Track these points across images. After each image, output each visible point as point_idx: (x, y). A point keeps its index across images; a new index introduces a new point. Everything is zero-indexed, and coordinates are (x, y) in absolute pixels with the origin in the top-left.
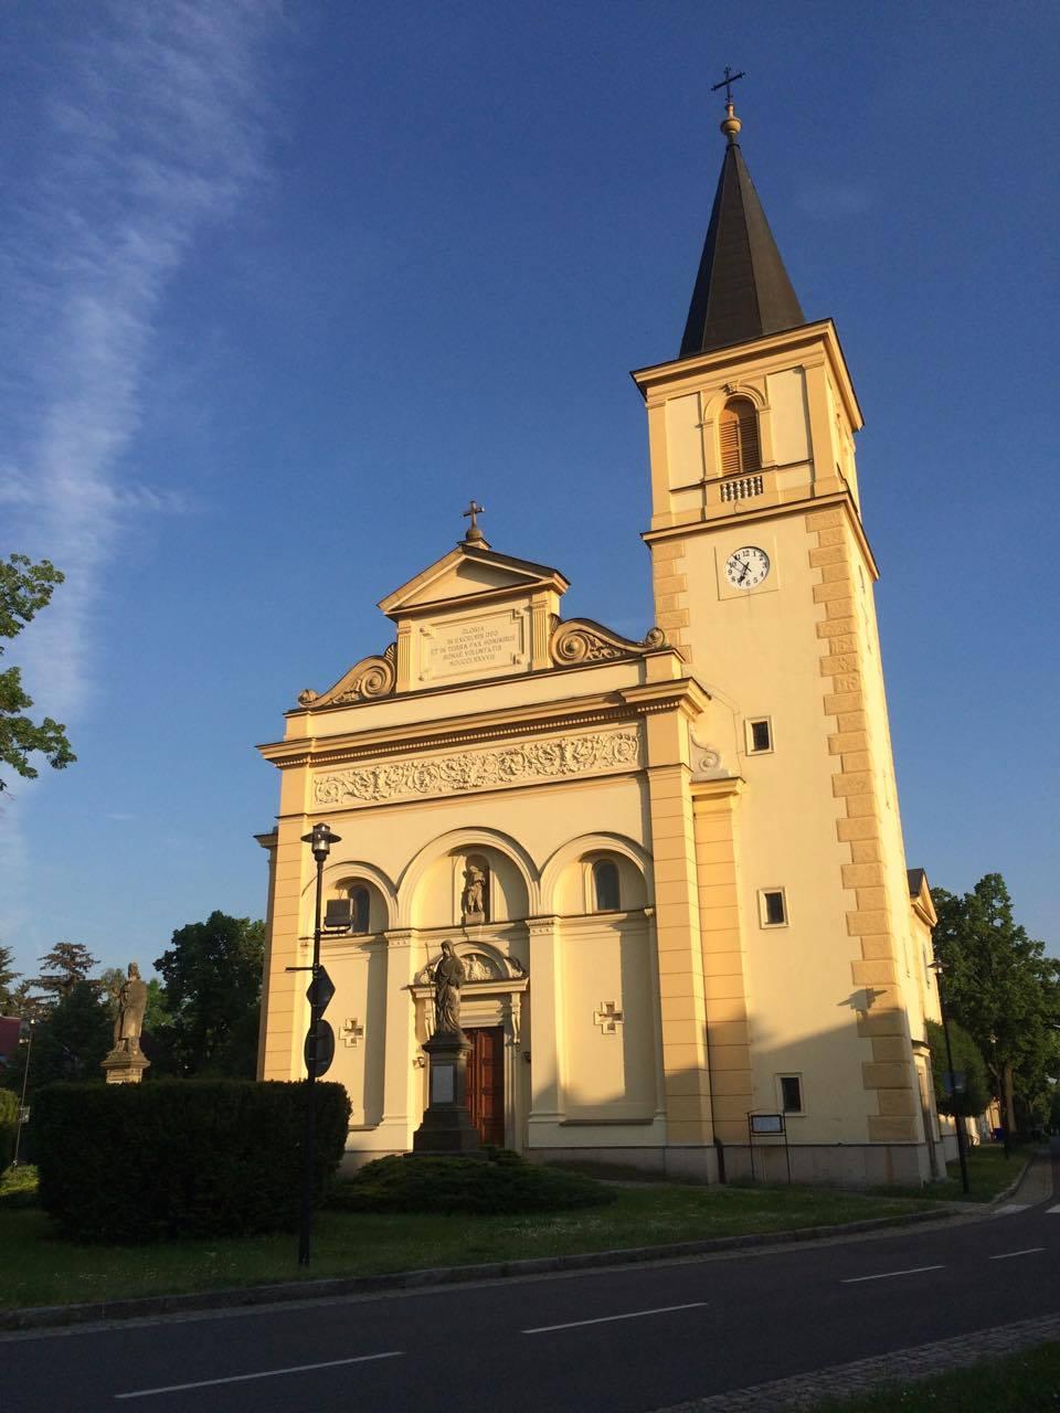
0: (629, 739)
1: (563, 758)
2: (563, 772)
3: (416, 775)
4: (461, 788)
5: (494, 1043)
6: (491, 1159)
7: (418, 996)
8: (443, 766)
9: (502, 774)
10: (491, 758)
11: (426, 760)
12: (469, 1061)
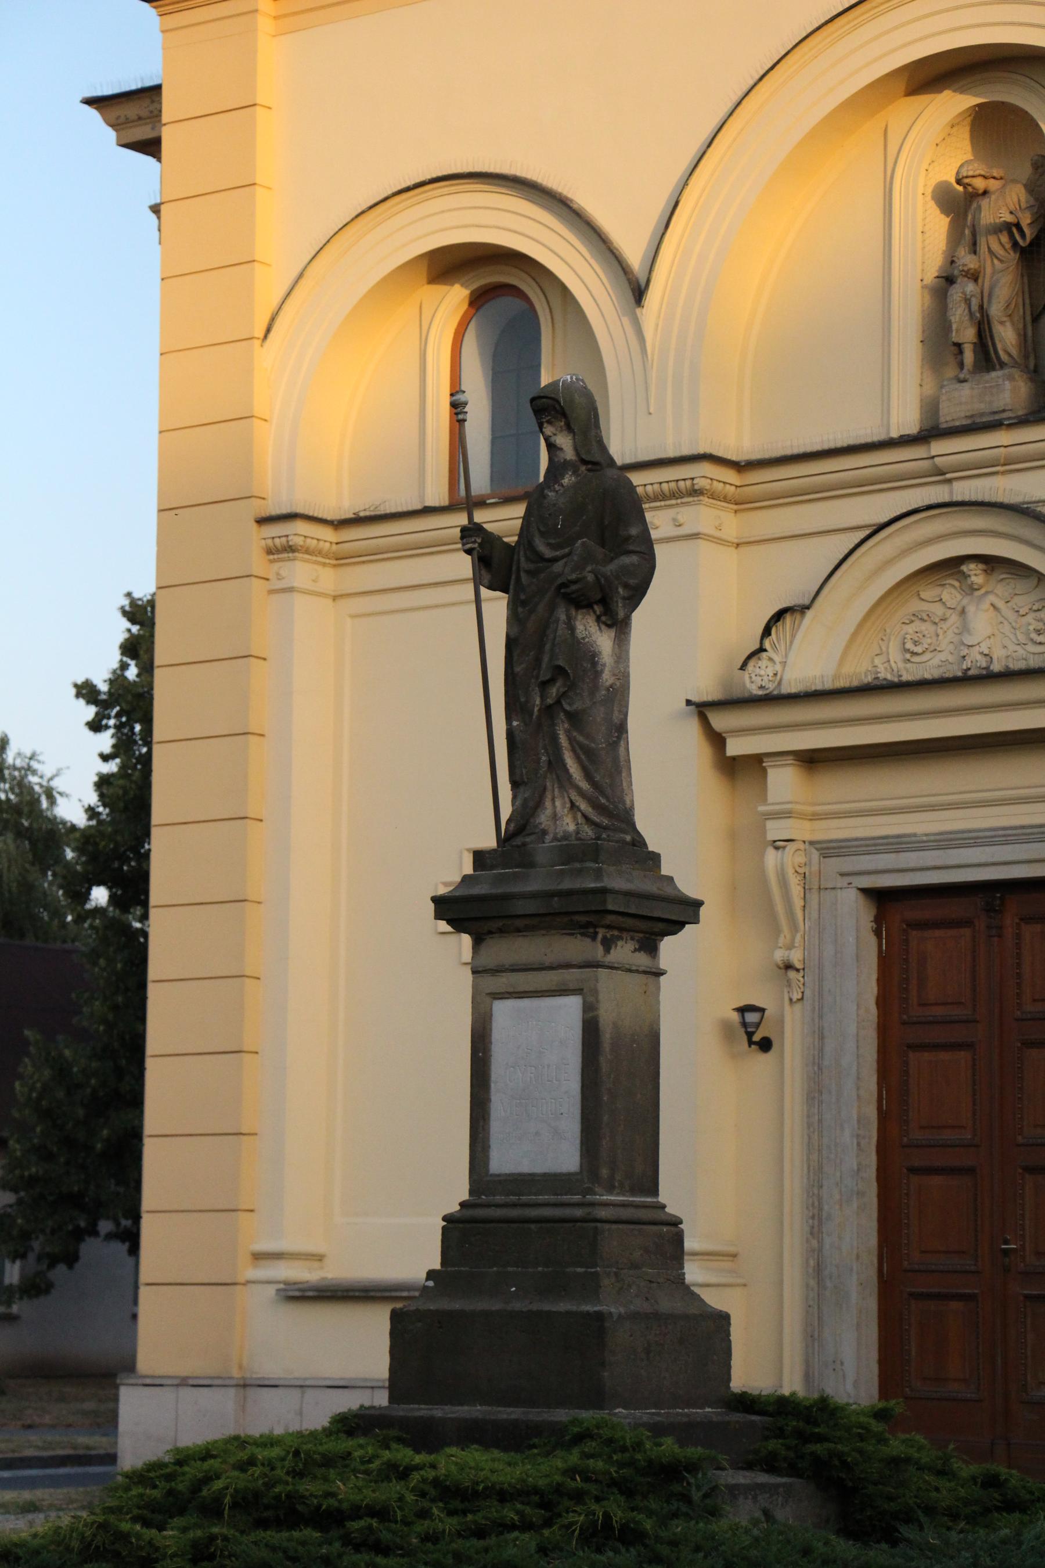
7: (735, 747)
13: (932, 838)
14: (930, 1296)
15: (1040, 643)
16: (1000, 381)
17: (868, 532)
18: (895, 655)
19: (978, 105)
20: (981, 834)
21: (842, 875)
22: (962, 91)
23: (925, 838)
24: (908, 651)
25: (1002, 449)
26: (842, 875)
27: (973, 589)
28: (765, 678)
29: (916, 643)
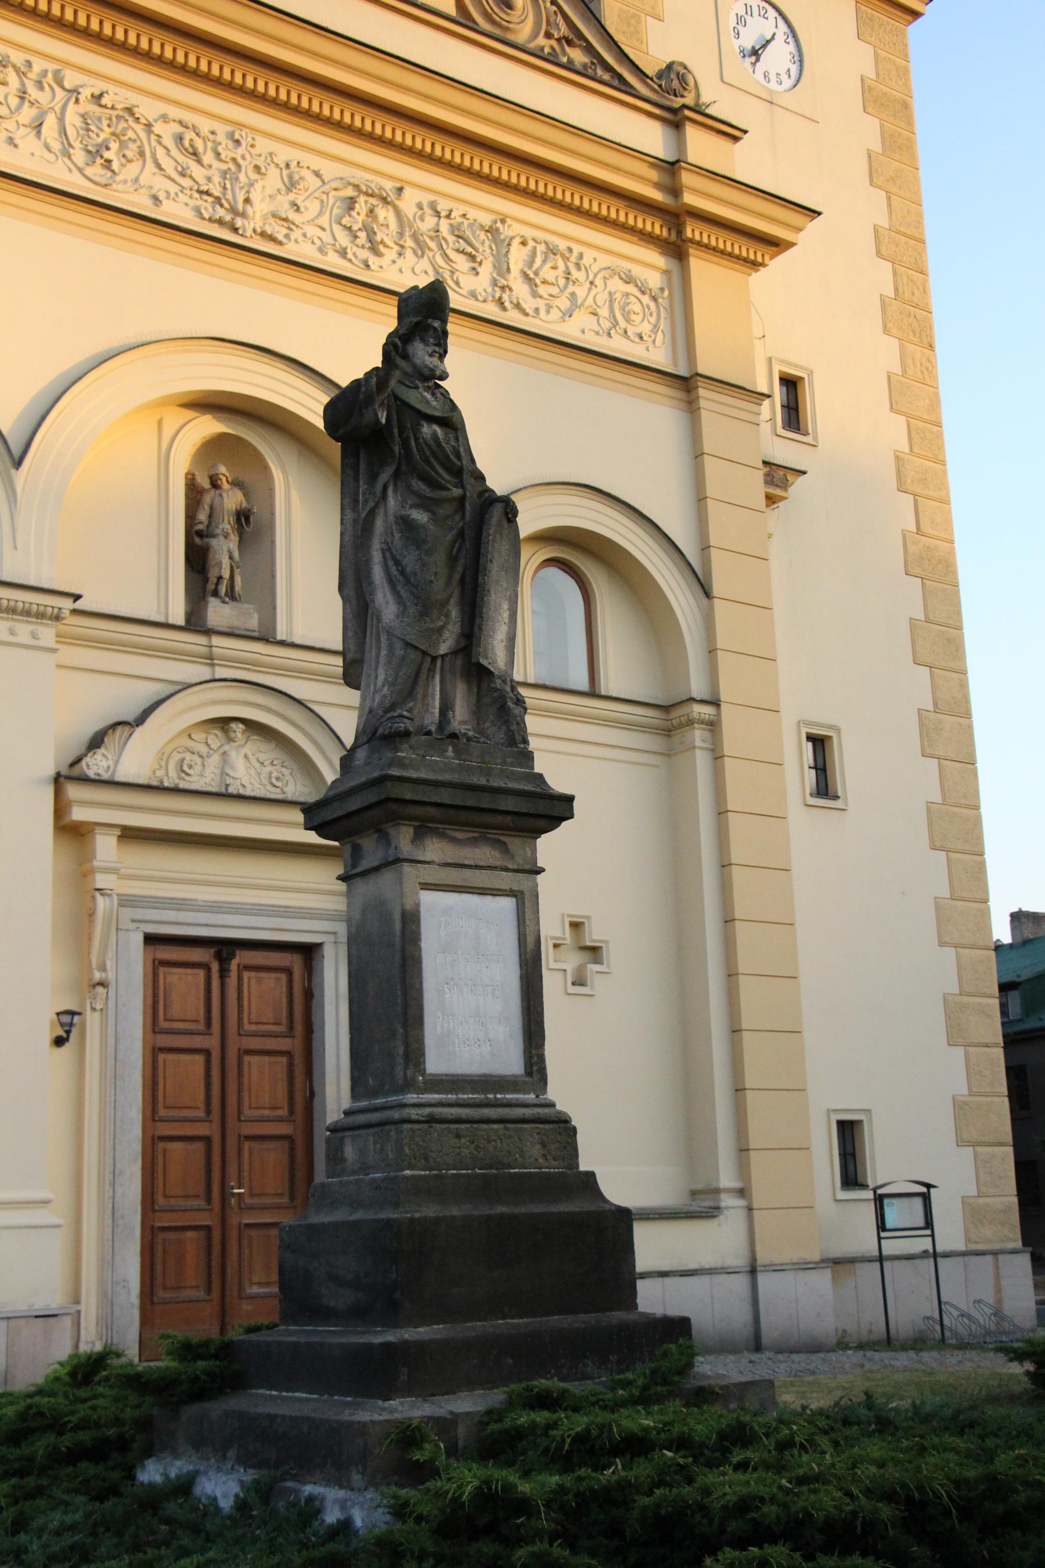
0: (643, 293)
1: (502, 268)
2: (500, 303)
3: (72, 118)
4: (220, 222)
5: (29, 9)
6: (313, 1536)
7: (78, 814)
8: (167, 132)
9: (343, 239)
10: (313, 182)
11: (112, 88)
12: (166, 1524)
13: (208, 904)
14: (170, 1229)
15: (275, 786)
16: (251, 611)
17: (181, 687)
18: (173, 773)
19: (225, 434)
20: (224, 905)
21: (133, 921)
22: (219, 420)
23: (203, 904)
24: (184, 772)
25: (258, 655)
26: (133, 921)
27: (230, 740)
28: (101, 768)
29: (190, 767)
